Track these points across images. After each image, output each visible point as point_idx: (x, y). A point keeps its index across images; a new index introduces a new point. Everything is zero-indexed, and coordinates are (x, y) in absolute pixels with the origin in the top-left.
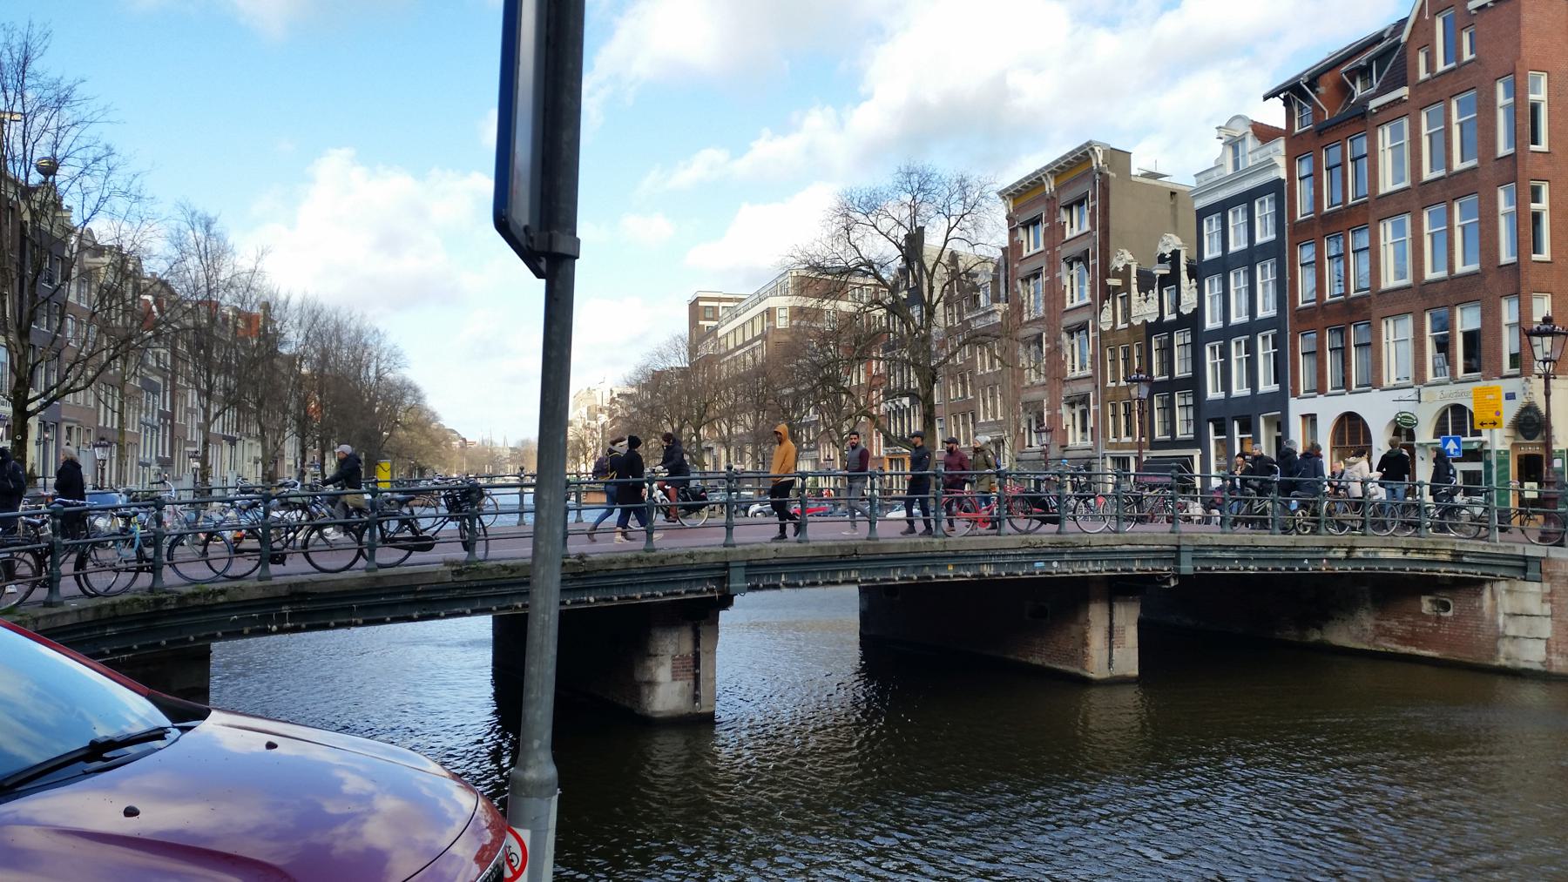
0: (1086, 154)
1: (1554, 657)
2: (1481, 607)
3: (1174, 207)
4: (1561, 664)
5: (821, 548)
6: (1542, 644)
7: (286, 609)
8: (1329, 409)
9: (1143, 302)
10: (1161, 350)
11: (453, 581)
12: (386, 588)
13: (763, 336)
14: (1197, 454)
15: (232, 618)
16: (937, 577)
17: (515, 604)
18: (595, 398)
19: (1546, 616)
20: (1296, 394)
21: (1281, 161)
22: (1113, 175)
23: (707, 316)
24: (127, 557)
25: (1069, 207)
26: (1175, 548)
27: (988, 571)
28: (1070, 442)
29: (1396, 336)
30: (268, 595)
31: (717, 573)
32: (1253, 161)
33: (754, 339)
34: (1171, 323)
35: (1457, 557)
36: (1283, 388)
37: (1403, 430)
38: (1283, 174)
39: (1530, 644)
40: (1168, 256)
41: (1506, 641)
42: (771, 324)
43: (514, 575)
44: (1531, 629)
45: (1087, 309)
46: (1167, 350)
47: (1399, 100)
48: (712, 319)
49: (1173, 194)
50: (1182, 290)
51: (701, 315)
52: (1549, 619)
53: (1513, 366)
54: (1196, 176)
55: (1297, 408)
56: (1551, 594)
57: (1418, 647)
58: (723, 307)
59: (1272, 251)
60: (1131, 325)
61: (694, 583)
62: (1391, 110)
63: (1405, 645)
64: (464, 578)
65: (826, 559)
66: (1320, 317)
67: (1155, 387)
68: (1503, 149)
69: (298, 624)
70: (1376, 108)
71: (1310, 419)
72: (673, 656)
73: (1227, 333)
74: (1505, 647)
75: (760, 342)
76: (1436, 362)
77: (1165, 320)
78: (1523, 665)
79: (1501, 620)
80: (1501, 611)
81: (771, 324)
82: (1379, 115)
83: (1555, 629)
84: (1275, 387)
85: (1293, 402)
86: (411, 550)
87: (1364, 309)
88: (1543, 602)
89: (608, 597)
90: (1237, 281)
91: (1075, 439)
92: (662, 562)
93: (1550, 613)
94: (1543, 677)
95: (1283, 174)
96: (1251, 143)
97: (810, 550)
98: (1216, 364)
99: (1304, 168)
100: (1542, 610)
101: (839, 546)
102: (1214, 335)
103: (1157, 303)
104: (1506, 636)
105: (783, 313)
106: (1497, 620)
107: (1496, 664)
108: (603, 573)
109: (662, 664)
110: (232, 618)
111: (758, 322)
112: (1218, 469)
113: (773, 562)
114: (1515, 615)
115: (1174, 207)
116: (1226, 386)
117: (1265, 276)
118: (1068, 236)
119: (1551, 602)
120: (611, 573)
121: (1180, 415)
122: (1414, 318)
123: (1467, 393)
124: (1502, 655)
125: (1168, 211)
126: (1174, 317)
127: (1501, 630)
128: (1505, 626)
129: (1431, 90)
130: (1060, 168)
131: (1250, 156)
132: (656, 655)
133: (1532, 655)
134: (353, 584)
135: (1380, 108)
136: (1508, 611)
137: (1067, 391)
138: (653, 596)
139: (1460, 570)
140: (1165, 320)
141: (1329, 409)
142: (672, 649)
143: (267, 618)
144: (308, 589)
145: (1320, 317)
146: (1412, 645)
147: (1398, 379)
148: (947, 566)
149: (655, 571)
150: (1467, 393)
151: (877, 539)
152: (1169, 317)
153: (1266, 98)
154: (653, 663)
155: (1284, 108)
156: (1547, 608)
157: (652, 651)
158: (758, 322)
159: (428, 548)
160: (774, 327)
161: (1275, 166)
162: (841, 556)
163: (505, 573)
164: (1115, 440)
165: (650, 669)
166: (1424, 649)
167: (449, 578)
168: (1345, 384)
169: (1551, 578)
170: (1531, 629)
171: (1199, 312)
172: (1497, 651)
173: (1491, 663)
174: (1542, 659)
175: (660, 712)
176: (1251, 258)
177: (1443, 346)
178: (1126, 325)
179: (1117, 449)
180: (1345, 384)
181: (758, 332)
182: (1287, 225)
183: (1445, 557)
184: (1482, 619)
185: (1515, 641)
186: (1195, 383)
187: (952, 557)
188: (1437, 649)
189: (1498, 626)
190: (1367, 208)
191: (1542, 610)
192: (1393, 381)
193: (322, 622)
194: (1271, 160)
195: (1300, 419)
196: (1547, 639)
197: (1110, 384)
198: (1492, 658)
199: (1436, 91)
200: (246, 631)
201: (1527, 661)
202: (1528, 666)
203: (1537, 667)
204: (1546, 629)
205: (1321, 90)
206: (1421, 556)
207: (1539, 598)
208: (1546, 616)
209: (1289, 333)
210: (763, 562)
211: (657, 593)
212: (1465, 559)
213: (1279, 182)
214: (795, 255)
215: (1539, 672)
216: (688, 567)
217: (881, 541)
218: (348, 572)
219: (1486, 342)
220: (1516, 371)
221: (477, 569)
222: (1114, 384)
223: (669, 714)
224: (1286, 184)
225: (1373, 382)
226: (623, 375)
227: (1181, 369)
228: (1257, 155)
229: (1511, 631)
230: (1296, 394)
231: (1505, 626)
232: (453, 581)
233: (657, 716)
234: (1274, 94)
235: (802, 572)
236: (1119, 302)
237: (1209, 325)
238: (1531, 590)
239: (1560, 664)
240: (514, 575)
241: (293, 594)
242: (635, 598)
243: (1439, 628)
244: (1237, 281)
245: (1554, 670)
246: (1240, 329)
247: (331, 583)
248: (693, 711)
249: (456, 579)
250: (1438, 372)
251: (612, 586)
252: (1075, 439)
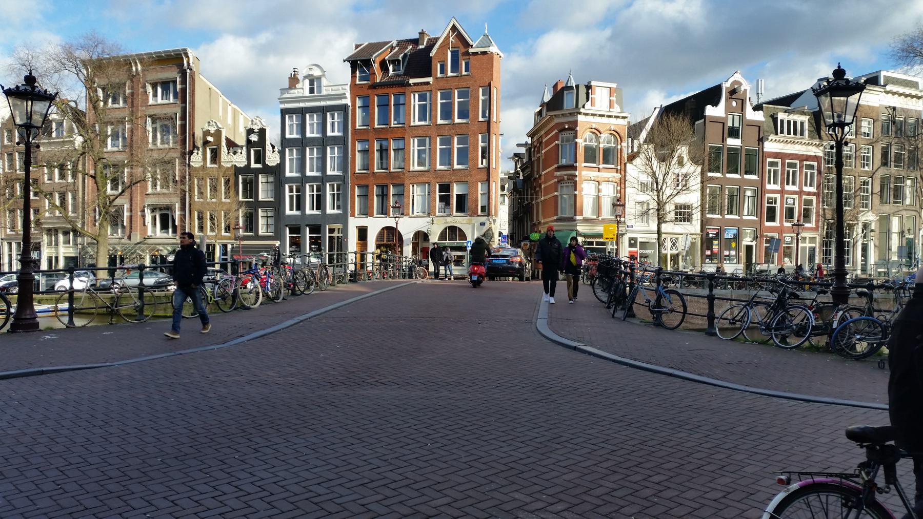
20: (353, 215)
24: (175, 107)
28: (150, 233)
47: (428, 83)
54: (280, 89)
59: (341, 142)
71: (363, 233)
85: (351, 220)
87: (401, 178)
95: (348, 101)
112: (291, 252)
116: (300, 206)
117: (333, 154)
122: (884, 467)
135: (415, 84)
141: (375, 225)
145: (372, 178)
161: (346, 98)
182: (350, 129)
209: (350, 185)
213: (346, 106)
224: (351, 108)
226: (661, 105)
230: (353, 215)
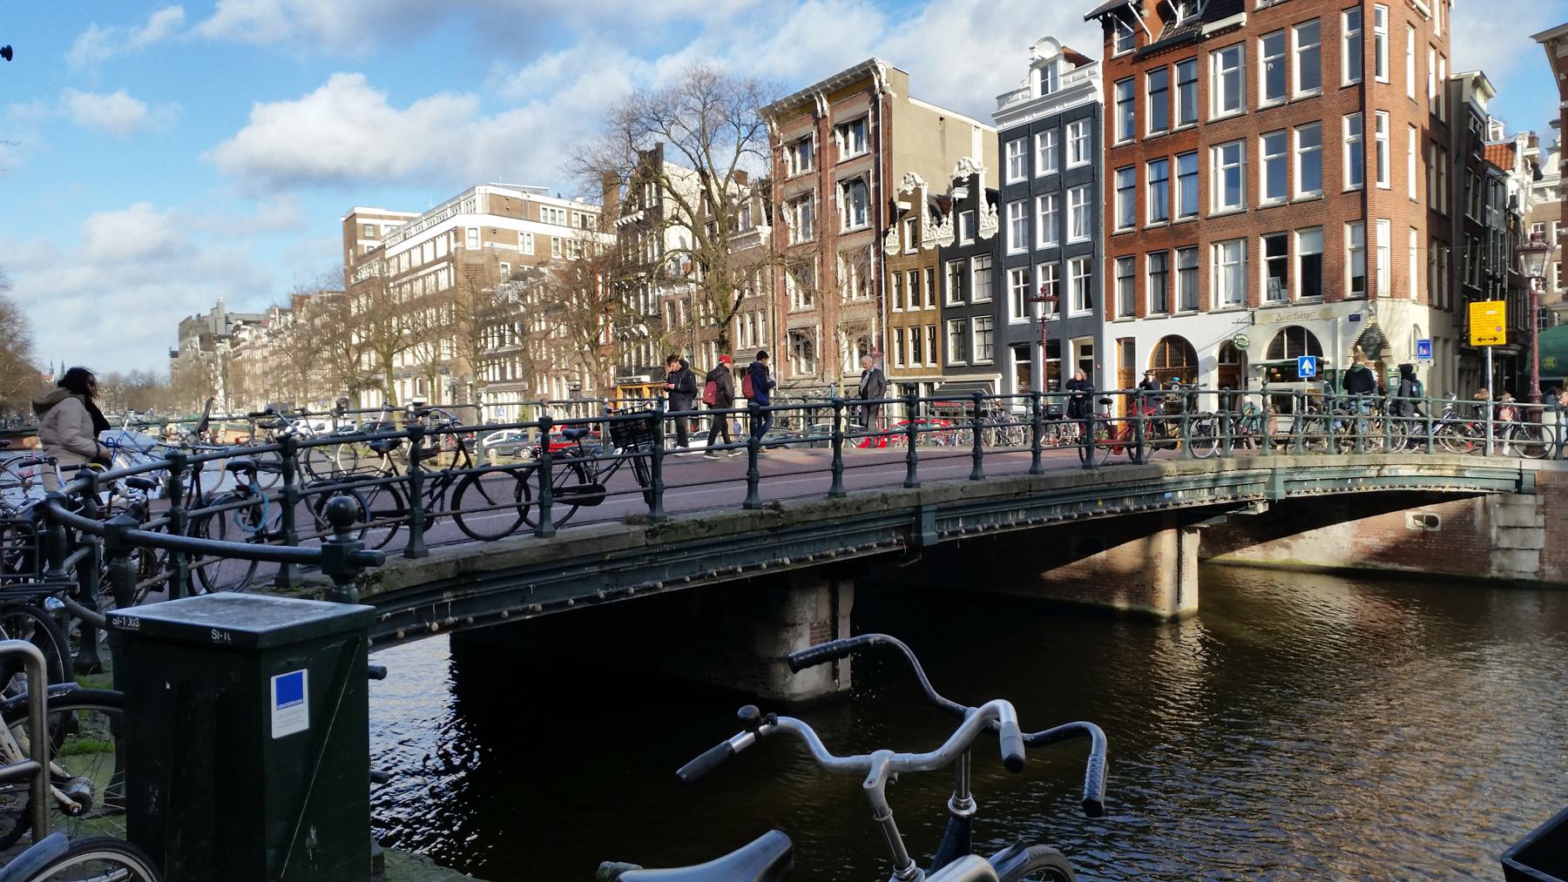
0: (868, 72)
1: (1546, 567)
2: (1472, 521)
3: (943, 132)
4: (1553, 573)
5: (1001, 485)
6: (1536, 555)
7: (448, 597)
8: (1149, 333)
9: (935, 227)
10: (955, 275)
11: (647, 545)
12: (572, 558)
13: (450, 258)
14: (998, 378)
15: (384, 616)
16: (1094, 514)
17: (709, 571)
18: (208, 326)
19: (1541, 528)
20: (1110, 318)
21: (1098, 83)
22: (894, 95)
23: (367, 234)
25: (844, 129)
26: (1270, 471)
27: (1131, 505)
29: (1221, 263)
30: (434, 578)
31: (905, 521)
32: (1065, 83)
33: (437, 261)
34: (967, 248)
35: (1460, 474)
36: (1098, 314)
37: (1232, 357)
38: (1099, 97)
39: (1524, 555)
40: (966, 180)
41: (1499, 554)
42: (460, 244)
43: (711, 533)
44: (1525, 540)
45: (868, 232)
46: (962, 277)
47: (1237, 27)
48: (373, 238)
49: (941, 119)
50: (981, 214)
51: (359, 234)
52: (1543, 530)
53: (1354, 289)
54: (998, 98)
55: (1112, 332)
56: (1545, 505)
57: (1401, 563)
58: (386, 226)
59: (1087, 178)
60: (922, 250)
61: (880, 534)
62: (1222, 38)
63: (1387, 562)
64: (659, 540)
65: (1003, 499)
66: (1141, 242)
67: (947, 313)
68: (1346, 81)
69: (463, 617)
70: (1209, 33)
71: (1129, 345)
72: (812, 624)
73: (1032, 258)
74: (1498, 559)
75: (445, 264)
76: (1271, 285)
77: (961, 245)
78: (1516, 576)
79: (1494, 532)
80: (1494, 524)
81: (460, 244)
82: (1212, 41)
83: (1548, 541)
84: (1084, 312)
86: (576, 504)
88: (1537, 513)
89: (803, 556)
90: (1043, 210)
91: (852, 366)
92: (858, 509)
93: (1543, 524)
94: (1536, 587)
95: (1099, 97)
96: (1063, 66)
97: (992, 488)
98: (1019, 289)
99: (1118, 94)
100: (1536, 521)
101: (1016, 482)
102: (1016, 260)
103: (952, 227)
104: (1499, 549)
105: (473, 233)
106: (1489, 533)
107: (1488, 576)
108: (800, 527)
109: (800, 635)
110: (384, 616)
111: (442, 242)
113: (958, 503)
114: (1509, 527)
115: (943, 132)
117: (1075, 203)
118: (843, 157)
119: (1544, 513)
120: (809, 526)
121: (977, 340)
123: (1307, 315)
124: (1494, 568)
125: (938, 136)
126: (971, 242)
127: (1493, 543)
128: (1498, 539)
129: (1269, 16)
130: (836, 86)
131: (1062, 78)
132: (794, 625)
133: (1526, 565)
134: (534, 555)
135: (1214, 34)
136: (1502, 523)
137: (844, 317)
138: (846, 553)
139: (1462, 485)
140: (961, 245)
142: (810, 616)
143: (423, 614)
144: (480, 565)
145: (1141, 242)
146: (1394, 561)
147: (1227, 302)
148: (1096, 501)
149: (850, 520)
150: (1307, 315)
151: (1043, 472)
152: (965, 242)
153: (1087, 19)
154: (791, 634)
155: (1102, 31)
156: (1541, 520)
157: (789, 620)
158: (442, 242)
159: (596, 501)
160: (464, 249)
161: (1093, 90)
162: (1017, 494)
163: (703, 533)
164: (901, 366)
165: (786, 642)
166: (1407, 565)
167: (643, 541)
168: (1164, 307)
169: (1545, 490)
170: (1525, 540)
171: (1000, 237)
172: (1489, 564)
173: (1480, 575)
174: (1535, 569)
175: (799, 694)
176: (1059, 185)
177: (1279, 270)
178: (915, 250)
179: (904, 375)
180: (1164, 307)
181: (442, 253)
182: (1104, 149)
183: (1450, 472)
184: (1472, 532)
185: (1509, 553)
186: (995, 309)
187: (1105, 491)
188: (1422, 564)
189: (1490, 539)
190: (1197, 133)
191: (1536, 521)
192: (1222, 304)
193: (492, 611)
194: (1089, 83)
195: (1116, 342)
196: (1541, 550)
197: (895, 309)
198: (1483, 570)
199: (1276, 18)
200: (401, 634)
201: (1521, 572)
202: (1521, 576)
203: (1532, 577)
204: (1539, 539)
205: (1145, 12)
206: (1431, 472)
207: (1534, 509)
208: (1541, 528)
209: (1104, 258)
210: (948, 505)
211: (850, 548)
212: (1467, 474)
214: (585, 158)
215: (1532, 582)
216: (881, 514)
217: (1047, 474)
218: (513, 538)
219: (1328, 264)
220: (1361, 294)
221: (672, 527)
222: (900, 310)
223: (808, 696)
225: (1195, 304)
227: (978, 293)
228: (1070, 78)
229: (1505, 543)
230: (1110, 318)
231: (1498, 539)
232: (647, 545)
233: (796, 699)
234: (1094, 16)
235: (975, 516)
236: (906, 224)
237: (1011, 250)
238: (1525, 502)
239: (1552, 573)
240: (711, 533)
241: (462, 574)
242: (828, 557)
243: (1425, 544)
244: (1043, 210)
245: (1547, 579)
246: (1047, 255)
247: (508, 556)
248: (832, 689)
249: (651, 542)
250: (1272, 294)
251: (629, 549)
252: (852, 366)
